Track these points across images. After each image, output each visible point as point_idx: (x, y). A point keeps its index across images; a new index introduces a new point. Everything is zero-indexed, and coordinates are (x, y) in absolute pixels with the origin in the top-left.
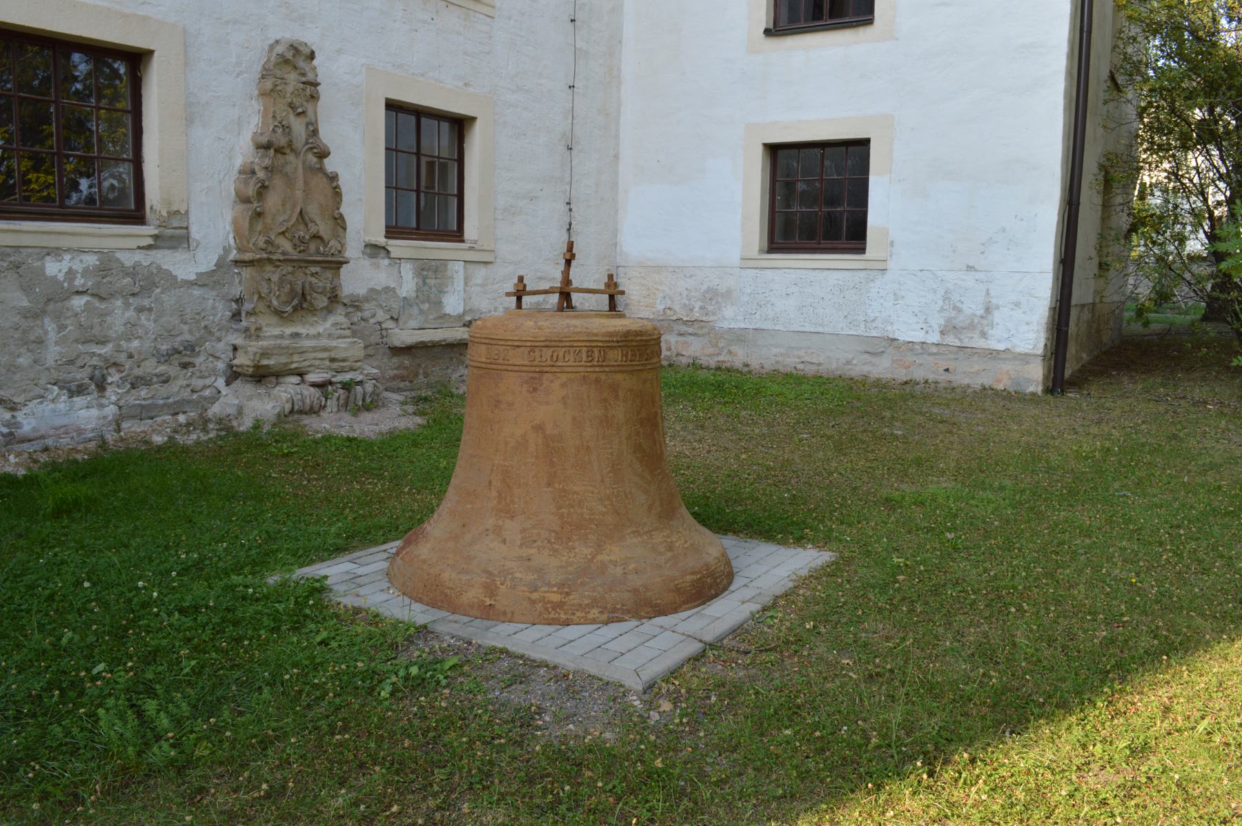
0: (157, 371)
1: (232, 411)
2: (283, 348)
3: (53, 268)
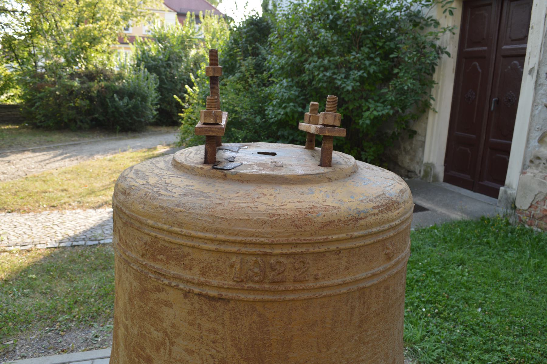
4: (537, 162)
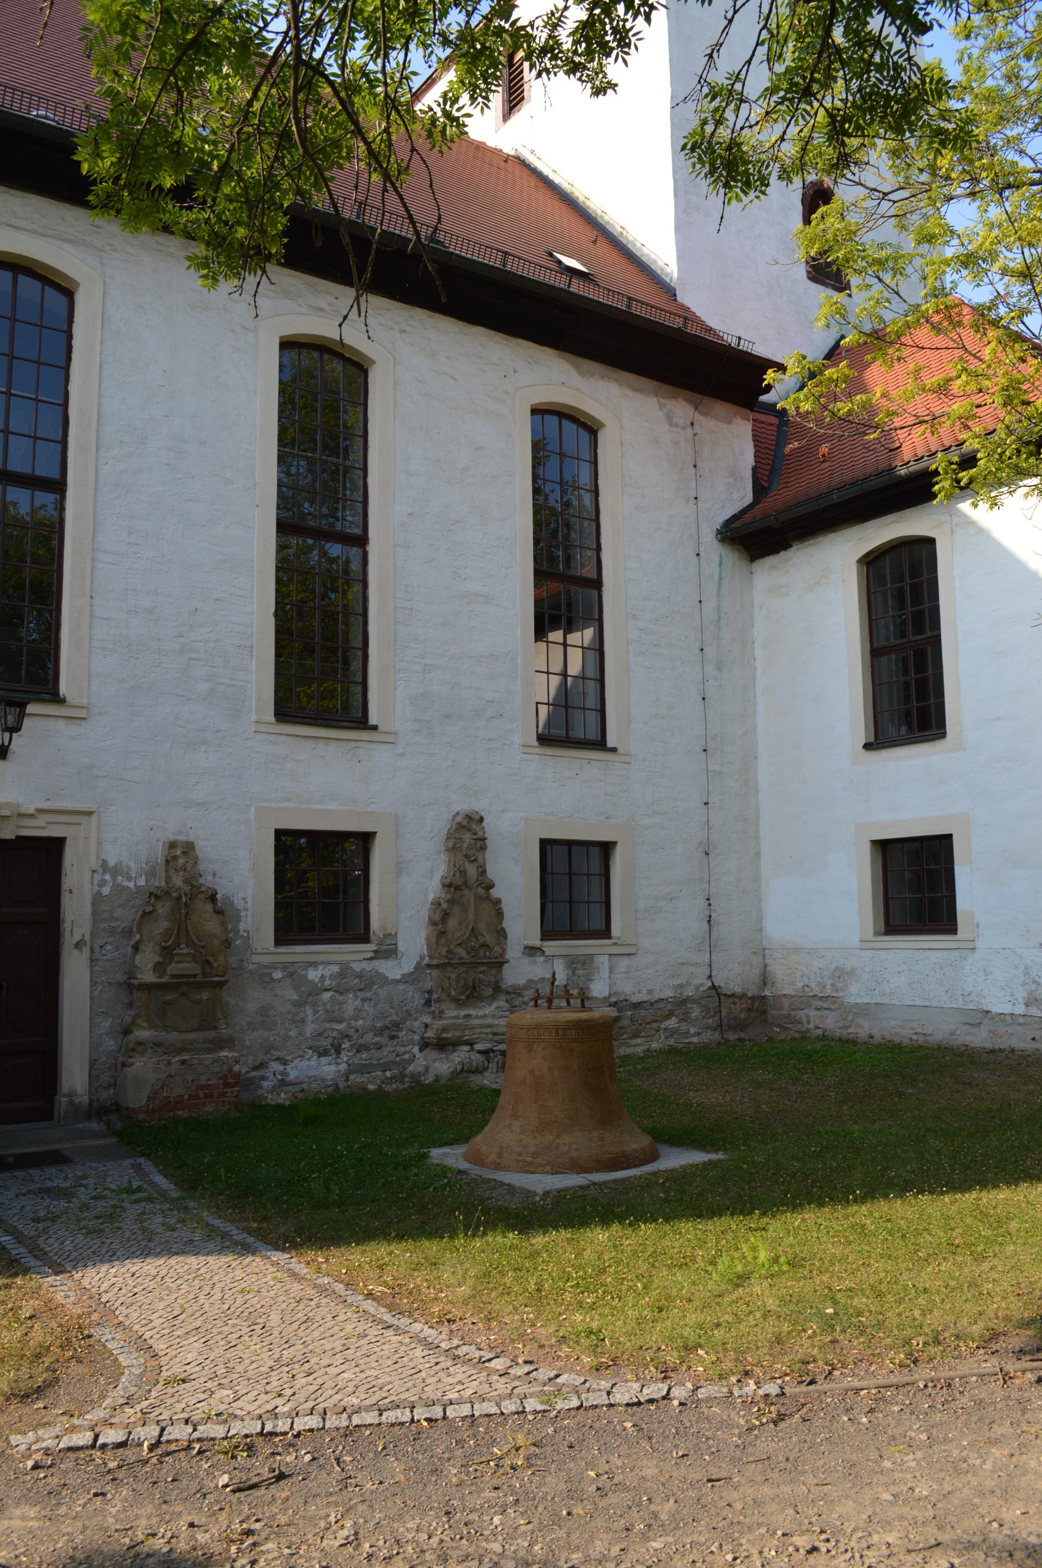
1: (421, 1069)
3: (313, 975)
4: (140, 1048)
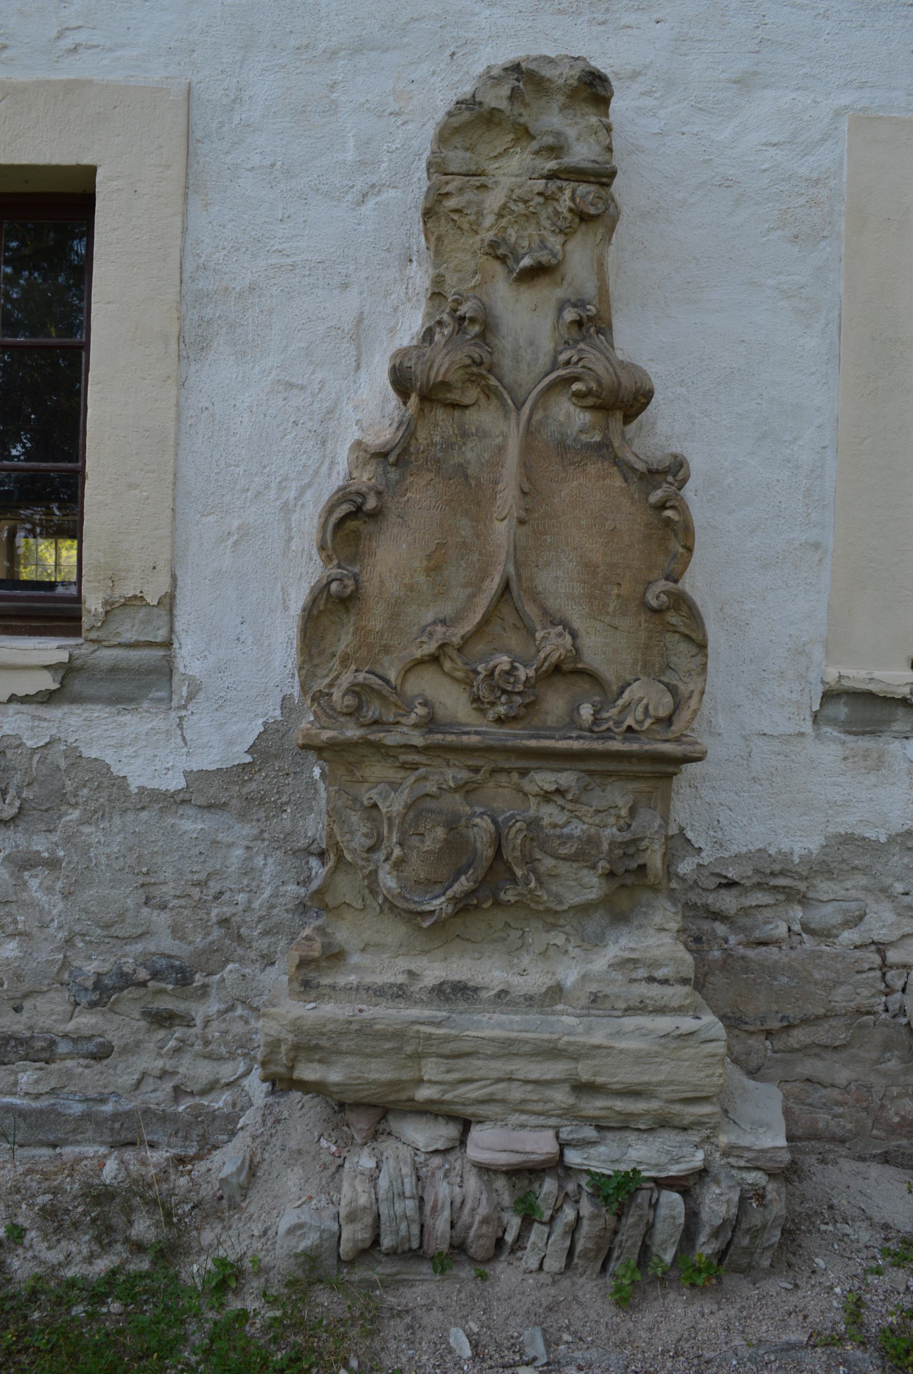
0: (70, 1026)
2: (382, 1036)
